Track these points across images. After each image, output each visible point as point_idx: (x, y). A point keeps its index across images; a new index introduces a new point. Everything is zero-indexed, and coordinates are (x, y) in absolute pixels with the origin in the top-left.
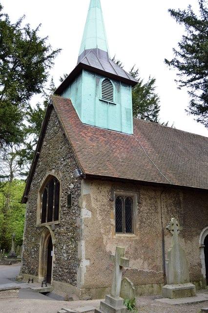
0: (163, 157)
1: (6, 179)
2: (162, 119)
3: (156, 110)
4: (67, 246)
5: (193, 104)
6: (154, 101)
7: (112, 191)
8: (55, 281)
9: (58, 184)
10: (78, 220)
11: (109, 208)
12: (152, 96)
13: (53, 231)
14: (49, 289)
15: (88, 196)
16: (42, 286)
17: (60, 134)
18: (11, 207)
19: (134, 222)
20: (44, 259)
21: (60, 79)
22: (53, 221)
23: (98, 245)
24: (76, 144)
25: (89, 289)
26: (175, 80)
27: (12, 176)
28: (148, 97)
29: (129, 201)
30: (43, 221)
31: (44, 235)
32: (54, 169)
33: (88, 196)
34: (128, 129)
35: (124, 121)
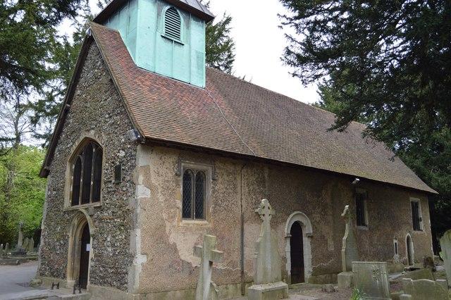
0: (243, 120)
1: (10, 145)
2: (238, 70)
3: (229, 60)
4: (114, 237)
5: (289, 52)
6: (227, 47)
7: (179, 162)
8: (93, 285)
9: (100, 152)
10: (131, 201)
11: (174, 184)
12: (225, 39)
13: (91, 216)
14: (85, 296)
15: (146, 168)
16: (74, 293)
17: (104, 80)
18: (16, 184)
19: (206, 205)
20: (76, 256)
21: (98, 3)
22: (91, 202)
23: (159, 236)
24: (130, 96)
25: (145, 294)
26: (278, 15)
27: (18, 139)
28: (221, 42)
29: (201, 177)
30: (75, 202)
31: (76, 222)
32: (93, 129)
33: (146, 168)
34: (199, 81)
35: (194, 69)
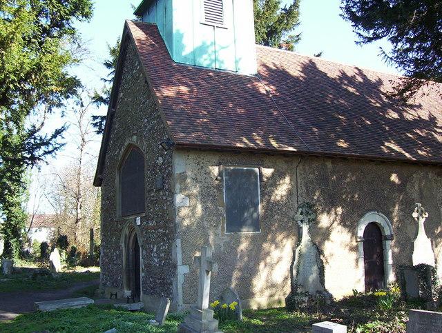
32: (134, 134)
